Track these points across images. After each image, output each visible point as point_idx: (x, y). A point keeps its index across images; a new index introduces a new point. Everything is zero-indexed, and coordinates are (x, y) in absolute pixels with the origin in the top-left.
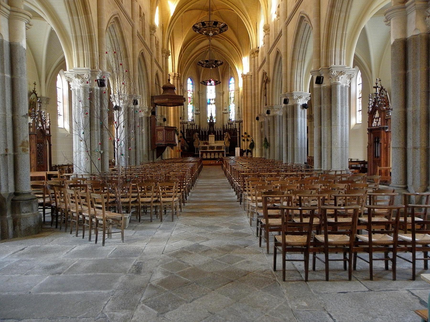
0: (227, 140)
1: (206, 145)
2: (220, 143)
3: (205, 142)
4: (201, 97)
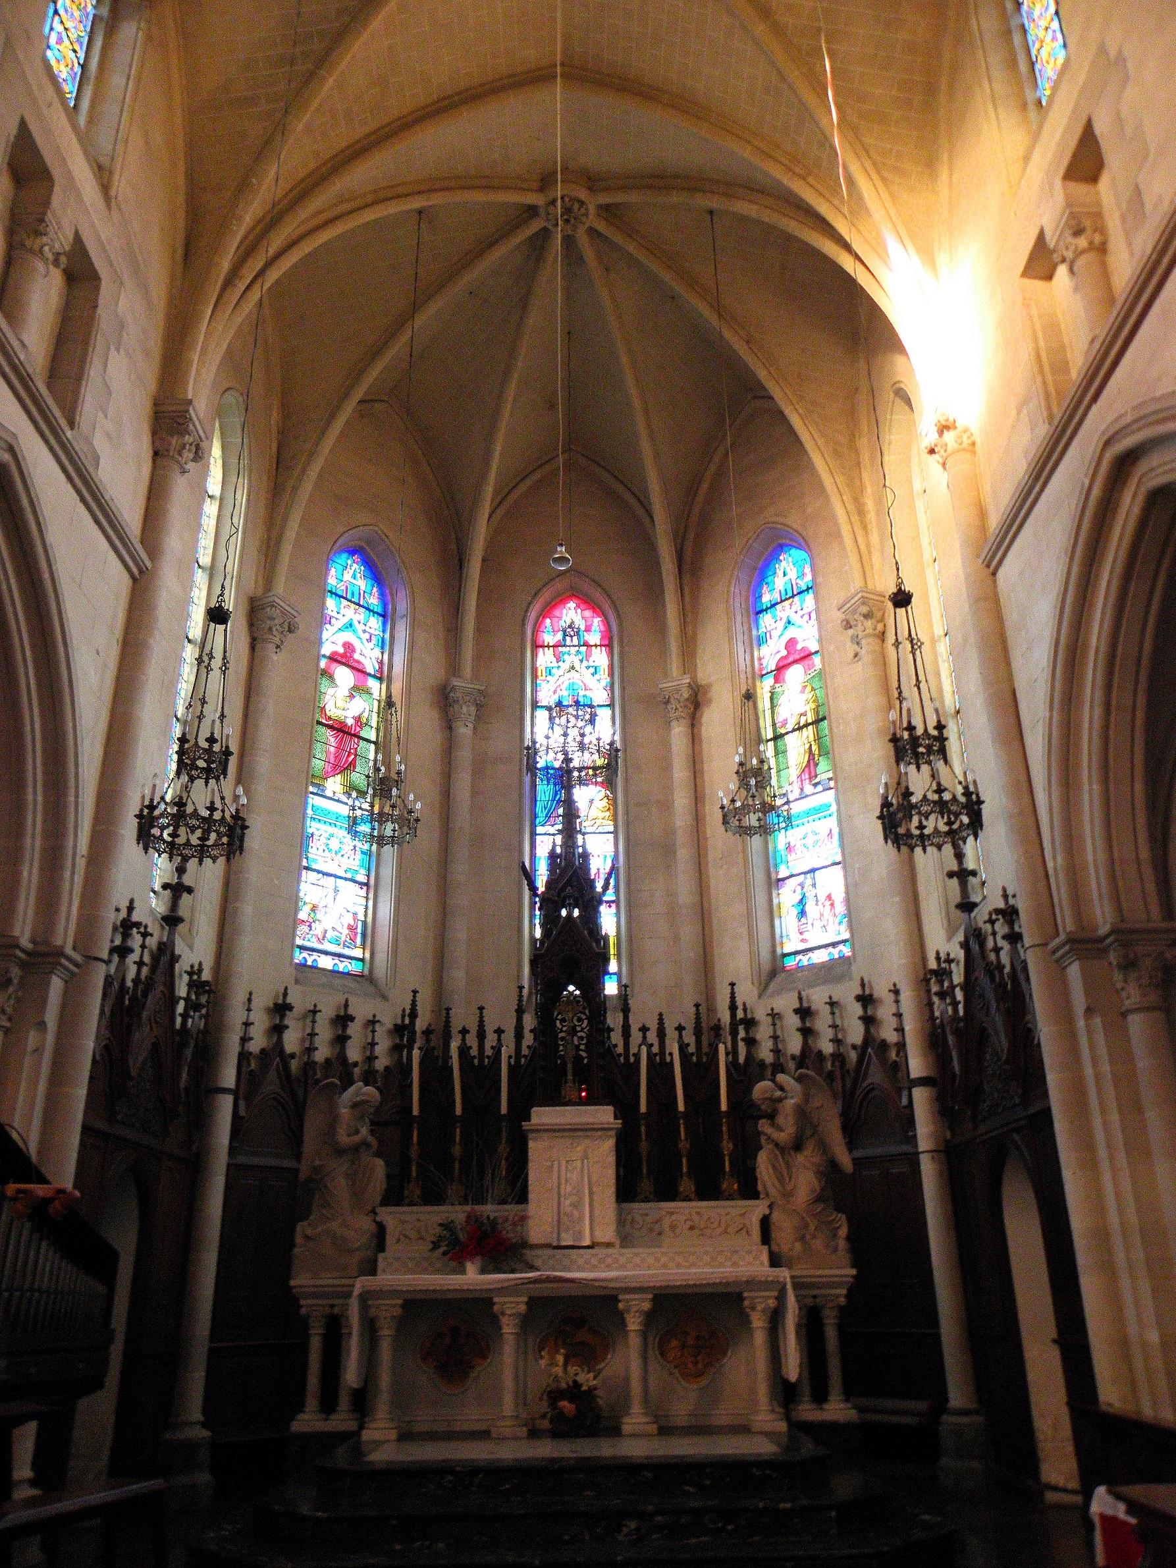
0: (805, 1181)
2: (704, 1246)
3: (458, 1213)
4: (464, 731)
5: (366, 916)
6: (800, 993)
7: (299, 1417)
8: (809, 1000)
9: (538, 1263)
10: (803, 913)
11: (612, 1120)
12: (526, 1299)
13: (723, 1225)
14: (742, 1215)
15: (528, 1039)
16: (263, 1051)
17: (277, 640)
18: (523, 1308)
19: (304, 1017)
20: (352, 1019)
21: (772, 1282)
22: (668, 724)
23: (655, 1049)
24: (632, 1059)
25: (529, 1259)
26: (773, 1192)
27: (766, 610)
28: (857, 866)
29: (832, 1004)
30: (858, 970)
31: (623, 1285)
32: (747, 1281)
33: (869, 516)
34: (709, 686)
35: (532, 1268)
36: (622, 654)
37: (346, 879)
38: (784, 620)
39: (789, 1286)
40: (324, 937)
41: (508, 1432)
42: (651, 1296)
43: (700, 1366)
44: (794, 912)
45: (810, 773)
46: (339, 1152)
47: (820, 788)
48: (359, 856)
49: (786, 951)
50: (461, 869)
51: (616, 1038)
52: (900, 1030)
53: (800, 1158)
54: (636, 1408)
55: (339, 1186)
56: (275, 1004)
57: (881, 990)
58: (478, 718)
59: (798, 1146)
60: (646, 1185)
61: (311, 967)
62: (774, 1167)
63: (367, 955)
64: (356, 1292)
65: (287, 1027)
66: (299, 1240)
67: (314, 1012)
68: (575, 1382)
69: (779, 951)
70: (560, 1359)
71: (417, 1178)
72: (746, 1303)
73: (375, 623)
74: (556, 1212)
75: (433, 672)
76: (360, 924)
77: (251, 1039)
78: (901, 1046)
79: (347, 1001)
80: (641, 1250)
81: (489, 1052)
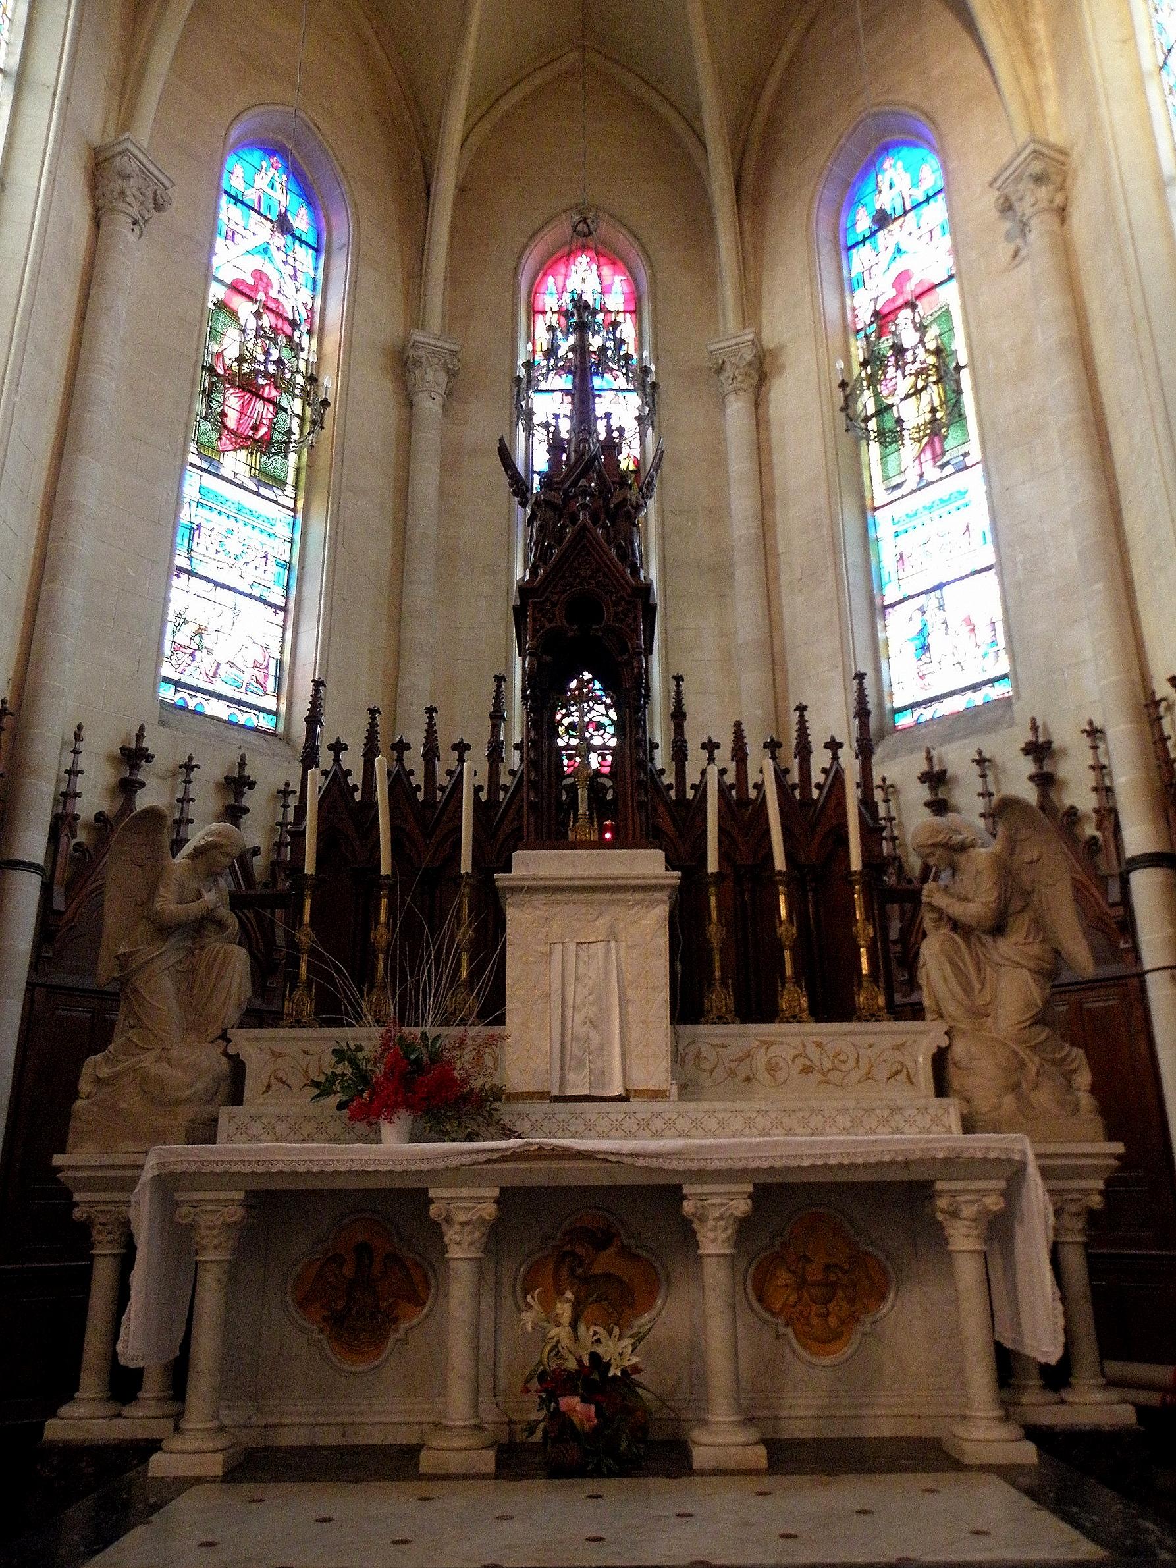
0: (1013, 991)
1: (394, 1148)
2: (826, 1099)
4: (430, 406)
5: (282, 652)
6: (928, 752)
7: (65, 1410)
8: (941, 760)
9: (523, 1126)
10: (925, 648)
11: (661, 870)
12: (496, 1192)
13: (864, 1064)
14: (899, 1048)
15: (514, 760)
16: (100, 816)
17: (134, 212)
18: (489, 1210)
19: (174, 775)
20: (252, 785)
21: (998, 1160)
22: (722, 405)
23: (730, 779)
24: (690, 794)
25: (506, 1120)
26: (951, 1008)
27: (863, 241)
28: (1020, 558)
29: (981, 761)
30: (1023, 713)
31: (695, 1165)
32: (946, 1161)
33: (1037, 48)
34: (780, 349)
35: (509, 1133)
36: (655, 313)
37: (251, 596)
38: (892, 248)
39: (1032, 1170)
40: (215, 674)
41: (456, 1462)
42: (749, 1188)
43: (833, 1321)
44: (911, 648)
45: (934, 452)
46: (164, 930)
47: (949, 469)
48: (273, 568)
49: (896, 705)
50: (421, 593)
51: (661, 758)
52: (1105, 791)
53: (1005, 947)
54: (722, 1413)
55: (162, 992)
56: (123, 749)
57: (1066, 735)
58: (450, 394)
59: (998, 928)
60: (720, 998)
61: (195, 712)
62: (952, 963)
63: (283, 707)
64: (146, 1175)
65: (142, 785)
66: (84, 1086)
67: (189, 767)
68: (594, 1356)
69: (888, 705)
70: (564, 1310)
71: (309, 982)
72: (942, 1203)
73: (304, 256)
74: (557, 1033)
75: (386, 325)
76: (273, 663)
77: (78, 795)
78: (1109, 816)
79: (243, 757)
80: (717, 1105)
81: (442, 779)
